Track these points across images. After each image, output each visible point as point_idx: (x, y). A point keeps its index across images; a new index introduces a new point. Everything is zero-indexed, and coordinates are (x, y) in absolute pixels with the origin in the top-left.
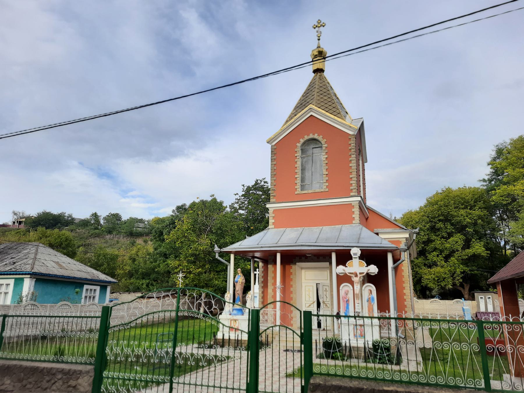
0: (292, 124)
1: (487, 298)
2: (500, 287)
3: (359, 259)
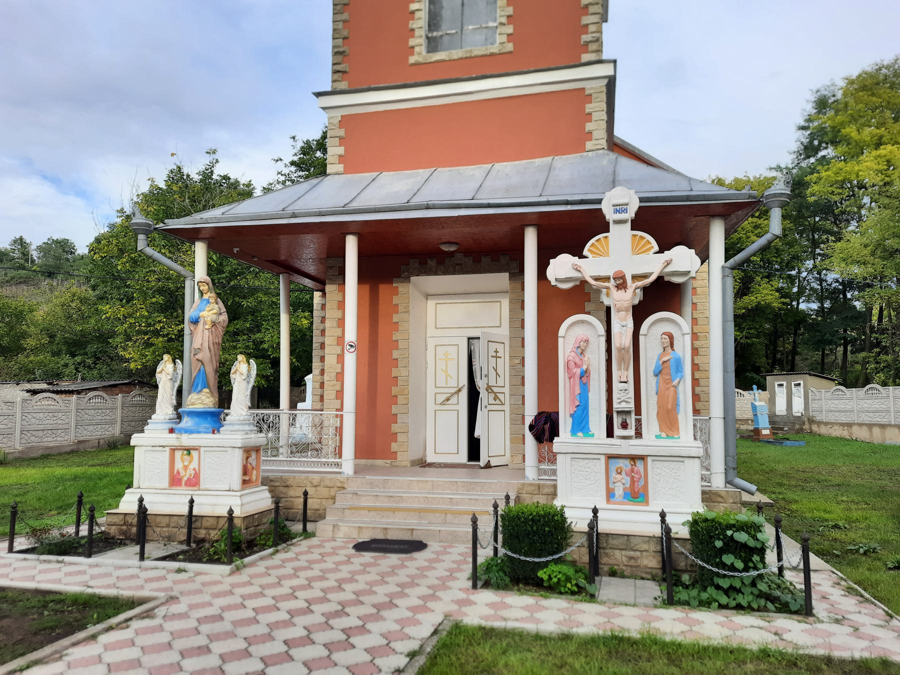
1: (793, 385)
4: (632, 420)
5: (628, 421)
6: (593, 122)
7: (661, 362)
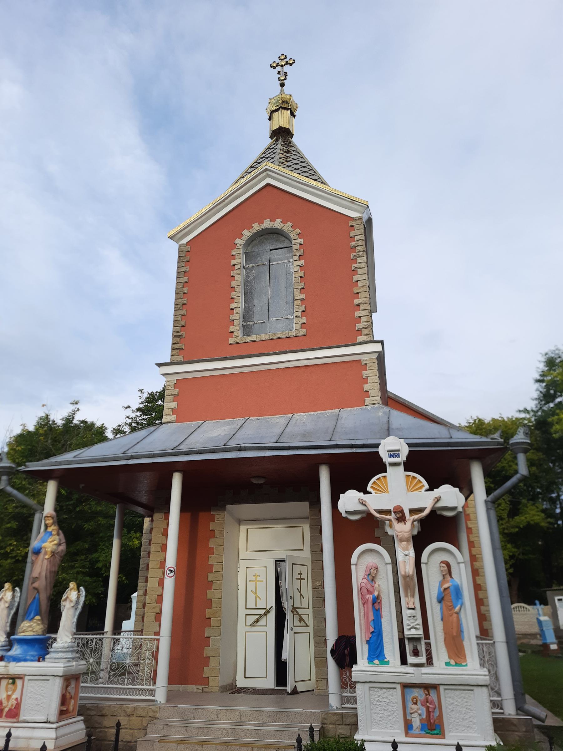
3: (406, 470)
4: (422, 648)
5: (419, 648)
6: (369, 384)
7: (442, 589)
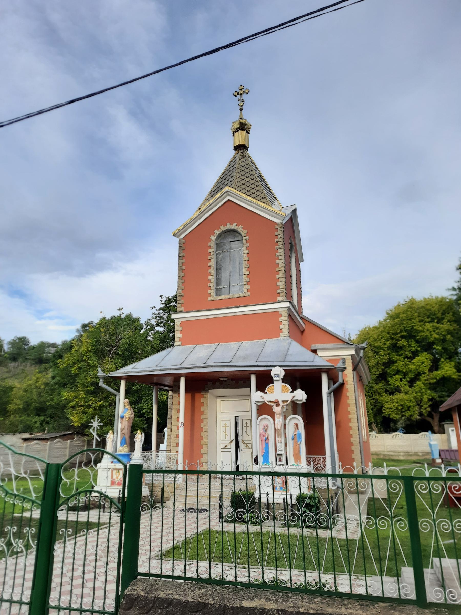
0: (205, 212)
2: (456, 417)
5: (281, 458)
